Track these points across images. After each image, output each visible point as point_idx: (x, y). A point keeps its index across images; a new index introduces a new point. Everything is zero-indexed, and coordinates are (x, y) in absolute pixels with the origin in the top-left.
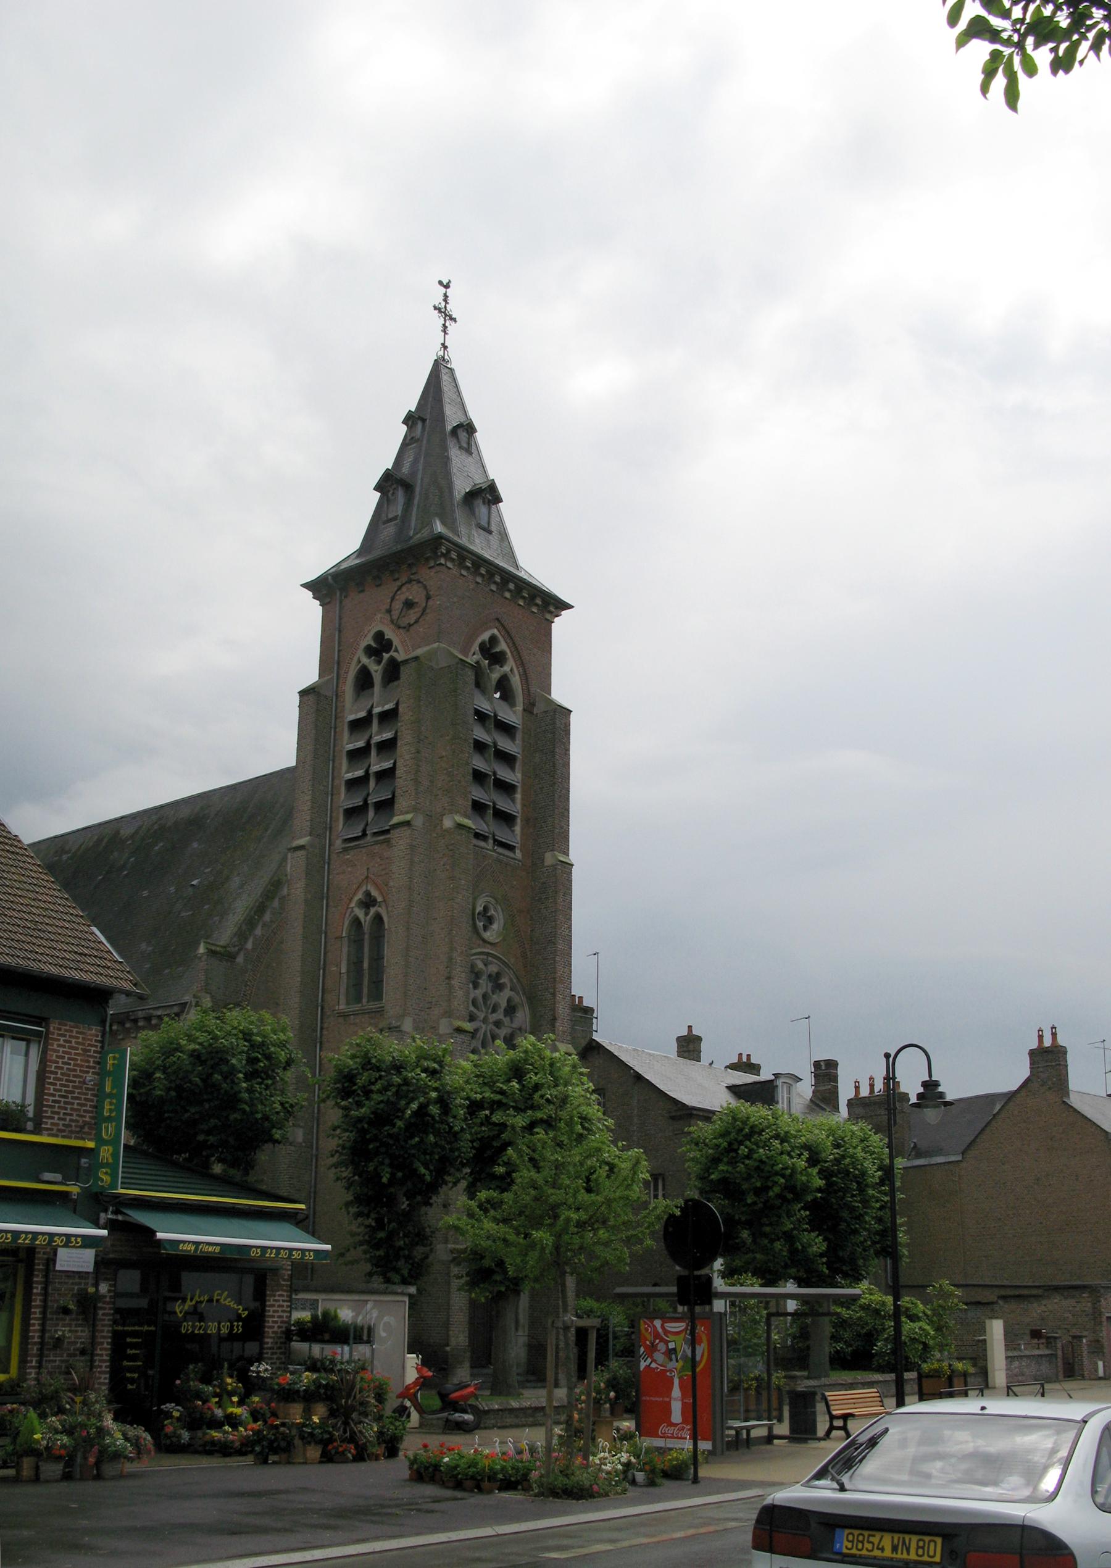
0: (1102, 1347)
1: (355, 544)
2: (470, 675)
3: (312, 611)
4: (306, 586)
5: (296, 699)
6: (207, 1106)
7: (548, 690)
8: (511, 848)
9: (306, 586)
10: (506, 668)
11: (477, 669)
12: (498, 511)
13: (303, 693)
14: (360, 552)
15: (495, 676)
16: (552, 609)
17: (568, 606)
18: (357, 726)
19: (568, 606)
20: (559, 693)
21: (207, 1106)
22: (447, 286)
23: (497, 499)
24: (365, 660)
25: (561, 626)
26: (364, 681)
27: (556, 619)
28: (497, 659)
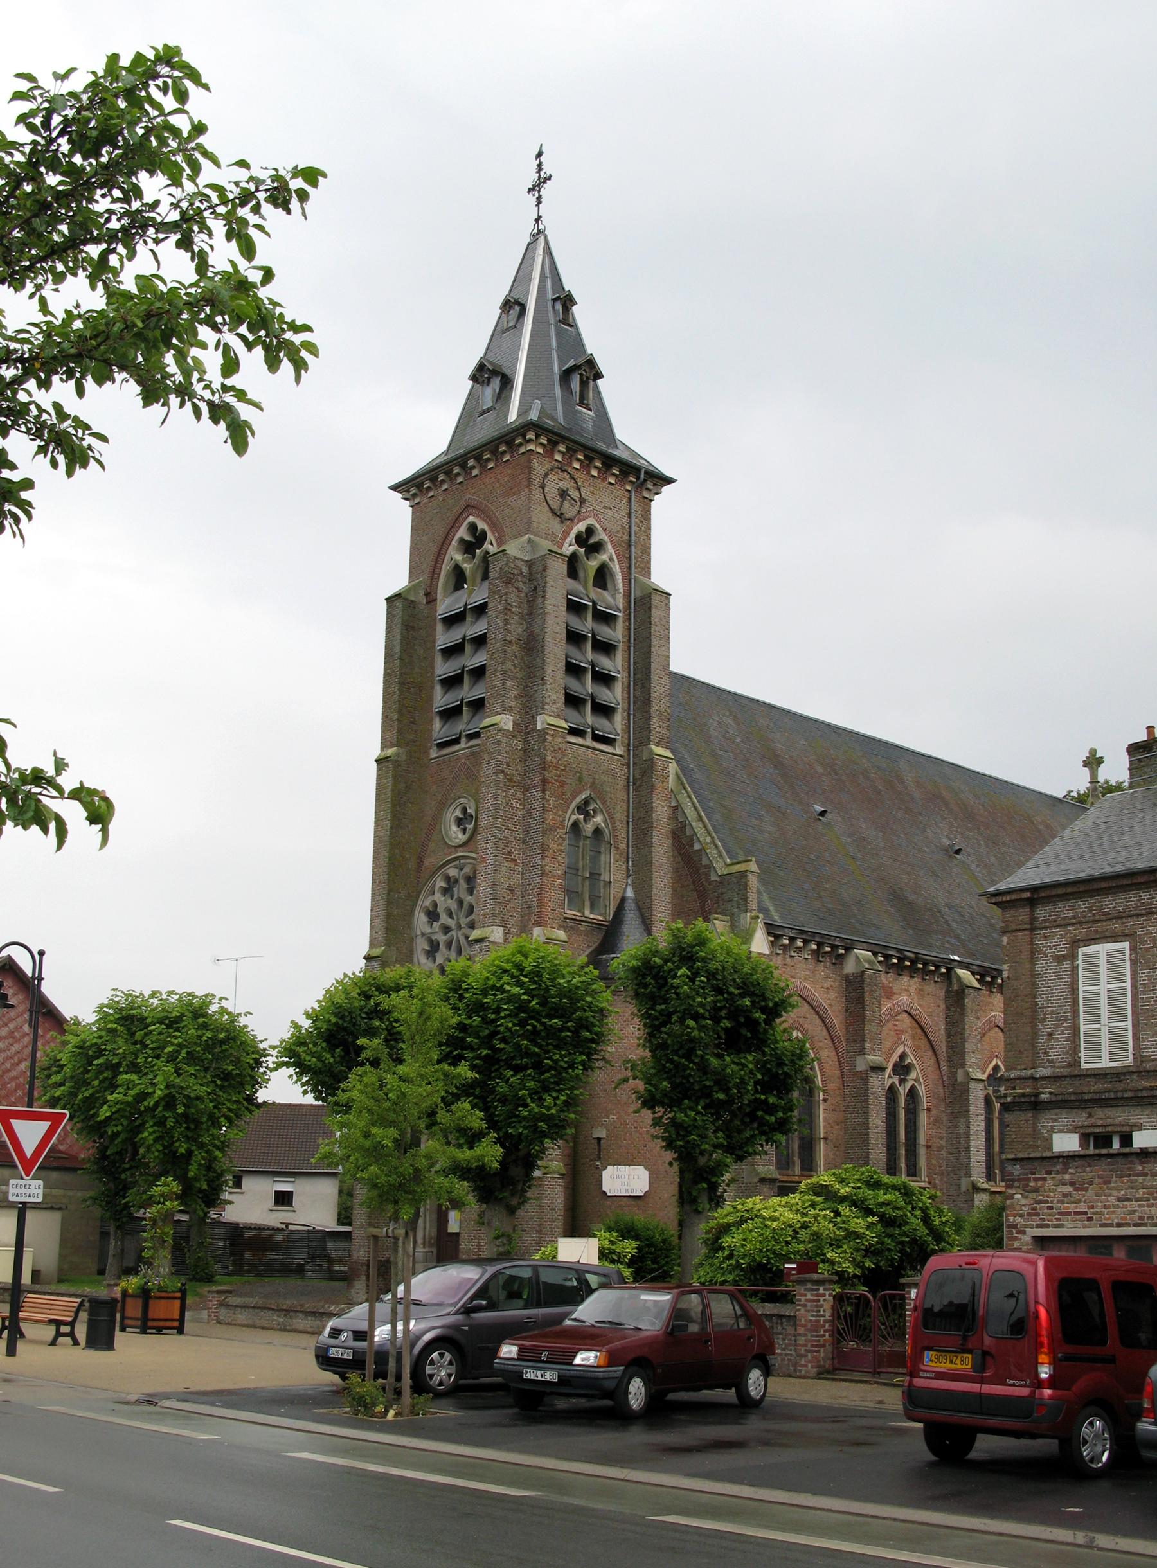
0: (783, 1076)
1: (444, 448)
2: (563, 567)
3: (401, 511)
4: (395, 488)
5: (384, 605)
6: (96, 1083)
7: (648, 574)
8: (609, 741)
9: (395, 488)
10: (604, 557)
11: (572, 560)
12: (598, 392)
13: (390, 600)
14: (446, 453)
15: (593, 564)
16: (650, 486)
17: (669, 481)
18: (453, 620)
19: (669, 481)
20: (659, 577)
21: (96, 1083)
22: (540, 154)
23: (598, 375)
24: (458, 557)
25: (662, 504)
26: (459, 578)
27: (656, 497)
28: (597, 548)
